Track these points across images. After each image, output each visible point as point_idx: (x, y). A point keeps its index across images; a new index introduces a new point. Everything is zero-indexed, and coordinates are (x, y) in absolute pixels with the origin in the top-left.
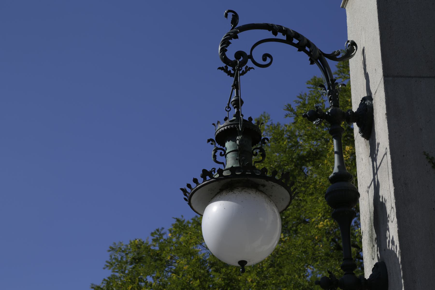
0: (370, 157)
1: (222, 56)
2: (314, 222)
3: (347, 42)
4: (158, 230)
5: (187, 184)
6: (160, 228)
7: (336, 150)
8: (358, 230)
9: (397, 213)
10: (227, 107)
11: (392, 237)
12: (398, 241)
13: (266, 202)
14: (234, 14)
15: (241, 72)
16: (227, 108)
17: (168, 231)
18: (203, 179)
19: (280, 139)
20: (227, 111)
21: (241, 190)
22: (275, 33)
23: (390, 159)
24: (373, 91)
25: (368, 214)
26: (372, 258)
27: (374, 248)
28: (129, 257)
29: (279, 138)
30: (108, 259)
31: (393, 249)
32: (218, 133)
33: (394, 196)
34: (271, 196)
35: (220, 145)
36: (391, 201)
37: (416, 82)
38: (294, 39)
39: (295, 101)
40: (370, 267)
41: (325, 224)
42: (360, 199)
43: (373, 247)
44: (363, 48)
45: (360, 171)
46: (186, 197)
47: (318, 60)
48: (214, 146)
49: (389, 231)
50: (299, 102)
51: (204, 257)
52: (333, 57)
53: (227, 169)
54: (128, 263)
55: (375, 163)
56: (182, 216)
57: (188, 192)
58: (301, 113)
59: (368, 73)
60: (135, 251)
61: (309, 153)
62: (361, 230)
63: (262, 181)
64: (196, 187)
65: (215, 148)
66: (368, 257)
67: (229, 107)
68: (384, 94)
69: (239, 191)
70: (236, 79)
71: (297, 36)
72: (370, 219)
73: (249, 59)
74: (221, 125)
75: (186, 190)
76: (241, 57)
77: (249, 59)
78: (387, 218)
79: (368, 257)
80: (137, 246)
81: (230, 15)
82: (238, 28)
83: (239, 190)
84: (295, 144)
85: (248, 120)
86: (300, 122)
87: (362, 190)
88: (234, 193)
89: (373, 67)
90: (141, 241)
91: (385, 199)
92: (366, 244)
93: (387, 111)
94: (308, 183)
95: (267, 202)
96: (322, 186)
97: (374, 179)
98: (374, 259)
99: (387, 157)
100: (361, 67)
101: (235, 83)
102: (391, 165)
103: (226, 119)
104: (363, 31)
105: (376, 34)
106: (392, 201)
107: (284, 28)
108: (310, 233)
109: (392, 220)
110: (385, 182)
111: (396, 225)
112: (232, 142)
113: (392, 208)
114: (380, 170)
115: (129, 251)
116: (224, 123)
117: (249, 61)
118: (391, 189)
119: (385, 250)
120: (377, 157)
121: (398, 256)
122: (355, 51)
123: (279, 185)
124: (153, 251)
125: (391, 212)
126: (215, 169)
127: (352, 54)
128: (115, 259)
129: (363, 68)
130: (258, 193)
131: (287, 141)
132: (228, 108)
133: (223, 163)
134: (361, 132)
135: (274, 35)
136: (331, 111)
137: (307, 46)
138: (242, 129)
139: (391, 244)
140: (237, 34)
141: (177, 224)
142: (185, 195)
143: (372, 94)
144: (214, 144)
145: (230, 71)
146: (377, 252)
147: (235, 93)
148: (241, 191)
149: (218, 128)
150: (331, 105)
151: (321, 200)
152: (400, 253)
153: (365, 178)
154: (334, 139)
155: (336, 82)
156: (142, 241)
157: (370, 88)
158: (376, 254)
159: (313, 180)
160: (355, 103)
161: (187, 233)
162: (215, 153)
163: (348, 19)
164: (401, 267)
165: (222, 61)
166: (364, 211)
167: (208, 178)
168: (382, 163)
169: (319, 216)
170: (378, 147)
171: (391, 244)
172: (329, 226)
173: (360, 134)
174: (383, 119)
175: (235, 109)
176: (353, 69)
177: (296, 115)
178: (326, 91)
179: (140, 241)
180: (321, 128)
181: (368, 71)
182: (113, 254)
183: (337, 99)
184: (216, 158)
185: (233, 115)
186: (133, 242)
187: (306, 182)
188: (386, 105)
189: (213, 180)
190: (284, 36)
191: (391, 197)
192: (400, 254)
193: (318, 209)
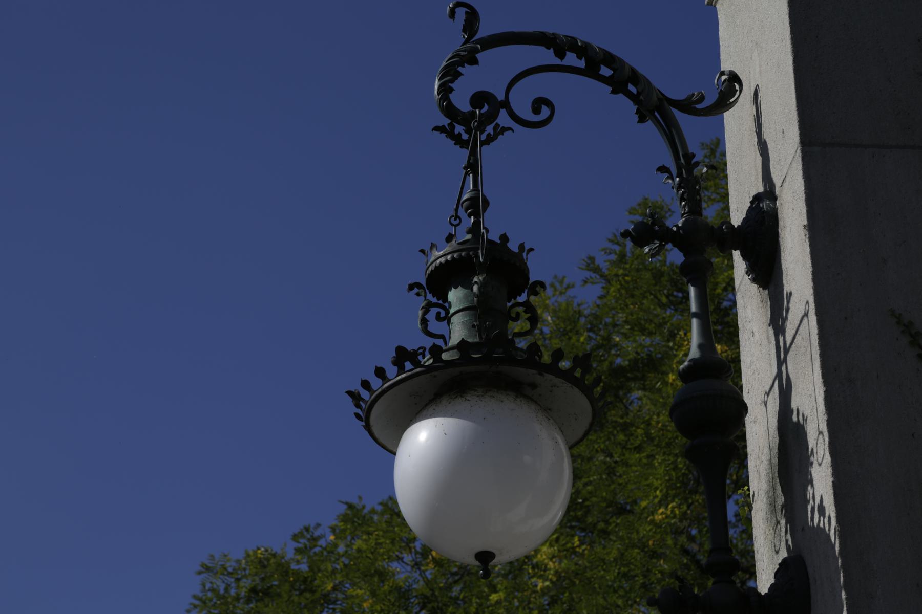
0: (771, 327)
1: (441, 103)
2: (644, 508)
3: (720, 74)
4: (307, 529)
5: (362, 380)
6: (312, 525)
7: (694, 308)
8: (743, 490)
9: (830, 443)
10: (453, 216)
11: (819, 499)
12: (834, 507)
13: (538, 420)
14: (468, 10)
15: (484, 137)
16: (453, 218)
17: (330, 530)
18: (396, 368)
19: (571, 331)
20: (452, 225)
21: (482, 394)
22: (560, 54)
23: (816, 325)
24: (777, 179)
25: (765, 452)
26: (774, 550)
27: (779, 527)
28: (242, 588)
29: (569, 328)
30: (197, 591)
31: (821, 525)
32: (432, 270)
33: (824, 407)
34: (550, 410)
35: (435, 298)
36: (818, 417)
37: (873, 156)
38: (602, 66)
39: (602, 250)
40: (770, 571)
41: (669, 512)
42: (748, 419)
43: (777, 525)
44: (756, 89)
45: (748, 359)
46: (359, 411)
47: (656, 114)
48: (422, 298)
49: (812, 486)
50: (612, 252)
51: (407, 584)
52: (688, 106)
53: (452, 348)
54: (242, 601)
55: (781, 339)
56: (360, 498)
57: (363, 400)
58: (617, 275)
59: (767, 140)
60: (256, 574)
61: (634, 363)
62: (748, 490)
63: (527, 374)
64: (381, 387)
65: (425, 302)
66: (765, 549)
67: (457, 217)
68: (803, 182)
69: (478, 396)
70: (473, 153)
71: (610, 59)
72: (771, 463)
73: (501, 110)
74: (438, 252)
75: (359, 395)
76: (486, 104)
77: (501, 110)
78: (809, 458)
79: (765, 549)
80: (260, 561)
81: (461, 12)
82: (478, 41)
83: (478, 394)
84: (605, 343)
85: (499, 242)
86: (614, 294)
87: (753, 401)
88: (466, 399)
89: (776, 127)
90: (270, 550)
91: (803, 416)
92: (761, 521)
93: (808, 221)
94: (632, 425)
95: (541, 421)
96: (663, 430)
97: (779, 375)
98: (780, 552)
99: (808, 321)
100: (751, 130)
101: (471, 161)
102: (818, 339)
103: (449, 238)
104: (756, 50)
105: (784, 52)
106: (819, 418)
107: (581, 41)
108: (638, 532)
109: (820, 460)
110: (804, 378)
111: (830, 470)
112: (463, 289)
113: (819, 434)
114: (794, 351)
115: (243, 573)
116: (445, 248)
117: (503, 113)
118: (817, 391)
119: (803, 529)
120: (785, 324)
121: (833, 539)
122: (738, 93)
123: (568, 383)
124: (297, 573)
125: (817, 443)
126: (425, 349)
127: (731, 100)
128: (212, 590)
129: (756, 131)
130: (521, 401)
131: (586, 334)
132: (455, 220)
133: (442, 337)
134: (750, 271)
135: (557, 58)
136: (684, 223)
137: (631, 83)
138: (484, 259)
139: (816, 515)
140: (476, 55)
141: (348, 515)
142: (358, 406)
143: (775, 187)
144: (423, 295)
145: (460, 134)
146: (786, 536)
147: (471, 183)
148: (482, 396)
149: (432, 259)
150: (685, 210)
151: (660, 461)
152: (837, 533)
153: (758, 374)
154: (690, 285)
155: (694, 161)
156: (273, 552)
157: (770, 174)
158: (782, 540)
159: (644, 418)
160: (738, 211)
161: (369, 534)
162: (425, 313)
163: (721, 29)
164: (840, 564)
165: (442, 113)
166: (757, 446)
167: (408, 365)
168: (797, 336)
169: (656, 497)
170: (788, 302)
171: (816, 515)
172: (678, 516)
173: (749, 276)
174: (800, 238)
175: (470, 217)
176: (732, 136)
177: (605, 280)
178: (673, 180)
179: (266, 550)
180: (660, 307)
181: (765, 136)
182: (209, 579)
183: (698, 197)
184: (427, 326)
185: (465, 230)
186: (251, 553)
187: (628, 421)
188: (807, 208)
189: (418, 370)
190: (581, 59)
191: (818, 410)
192: (838, 535)
193: (655, 481)
